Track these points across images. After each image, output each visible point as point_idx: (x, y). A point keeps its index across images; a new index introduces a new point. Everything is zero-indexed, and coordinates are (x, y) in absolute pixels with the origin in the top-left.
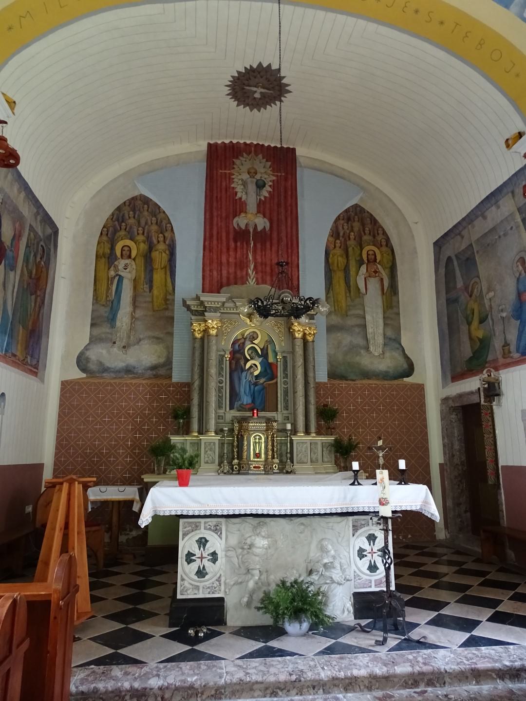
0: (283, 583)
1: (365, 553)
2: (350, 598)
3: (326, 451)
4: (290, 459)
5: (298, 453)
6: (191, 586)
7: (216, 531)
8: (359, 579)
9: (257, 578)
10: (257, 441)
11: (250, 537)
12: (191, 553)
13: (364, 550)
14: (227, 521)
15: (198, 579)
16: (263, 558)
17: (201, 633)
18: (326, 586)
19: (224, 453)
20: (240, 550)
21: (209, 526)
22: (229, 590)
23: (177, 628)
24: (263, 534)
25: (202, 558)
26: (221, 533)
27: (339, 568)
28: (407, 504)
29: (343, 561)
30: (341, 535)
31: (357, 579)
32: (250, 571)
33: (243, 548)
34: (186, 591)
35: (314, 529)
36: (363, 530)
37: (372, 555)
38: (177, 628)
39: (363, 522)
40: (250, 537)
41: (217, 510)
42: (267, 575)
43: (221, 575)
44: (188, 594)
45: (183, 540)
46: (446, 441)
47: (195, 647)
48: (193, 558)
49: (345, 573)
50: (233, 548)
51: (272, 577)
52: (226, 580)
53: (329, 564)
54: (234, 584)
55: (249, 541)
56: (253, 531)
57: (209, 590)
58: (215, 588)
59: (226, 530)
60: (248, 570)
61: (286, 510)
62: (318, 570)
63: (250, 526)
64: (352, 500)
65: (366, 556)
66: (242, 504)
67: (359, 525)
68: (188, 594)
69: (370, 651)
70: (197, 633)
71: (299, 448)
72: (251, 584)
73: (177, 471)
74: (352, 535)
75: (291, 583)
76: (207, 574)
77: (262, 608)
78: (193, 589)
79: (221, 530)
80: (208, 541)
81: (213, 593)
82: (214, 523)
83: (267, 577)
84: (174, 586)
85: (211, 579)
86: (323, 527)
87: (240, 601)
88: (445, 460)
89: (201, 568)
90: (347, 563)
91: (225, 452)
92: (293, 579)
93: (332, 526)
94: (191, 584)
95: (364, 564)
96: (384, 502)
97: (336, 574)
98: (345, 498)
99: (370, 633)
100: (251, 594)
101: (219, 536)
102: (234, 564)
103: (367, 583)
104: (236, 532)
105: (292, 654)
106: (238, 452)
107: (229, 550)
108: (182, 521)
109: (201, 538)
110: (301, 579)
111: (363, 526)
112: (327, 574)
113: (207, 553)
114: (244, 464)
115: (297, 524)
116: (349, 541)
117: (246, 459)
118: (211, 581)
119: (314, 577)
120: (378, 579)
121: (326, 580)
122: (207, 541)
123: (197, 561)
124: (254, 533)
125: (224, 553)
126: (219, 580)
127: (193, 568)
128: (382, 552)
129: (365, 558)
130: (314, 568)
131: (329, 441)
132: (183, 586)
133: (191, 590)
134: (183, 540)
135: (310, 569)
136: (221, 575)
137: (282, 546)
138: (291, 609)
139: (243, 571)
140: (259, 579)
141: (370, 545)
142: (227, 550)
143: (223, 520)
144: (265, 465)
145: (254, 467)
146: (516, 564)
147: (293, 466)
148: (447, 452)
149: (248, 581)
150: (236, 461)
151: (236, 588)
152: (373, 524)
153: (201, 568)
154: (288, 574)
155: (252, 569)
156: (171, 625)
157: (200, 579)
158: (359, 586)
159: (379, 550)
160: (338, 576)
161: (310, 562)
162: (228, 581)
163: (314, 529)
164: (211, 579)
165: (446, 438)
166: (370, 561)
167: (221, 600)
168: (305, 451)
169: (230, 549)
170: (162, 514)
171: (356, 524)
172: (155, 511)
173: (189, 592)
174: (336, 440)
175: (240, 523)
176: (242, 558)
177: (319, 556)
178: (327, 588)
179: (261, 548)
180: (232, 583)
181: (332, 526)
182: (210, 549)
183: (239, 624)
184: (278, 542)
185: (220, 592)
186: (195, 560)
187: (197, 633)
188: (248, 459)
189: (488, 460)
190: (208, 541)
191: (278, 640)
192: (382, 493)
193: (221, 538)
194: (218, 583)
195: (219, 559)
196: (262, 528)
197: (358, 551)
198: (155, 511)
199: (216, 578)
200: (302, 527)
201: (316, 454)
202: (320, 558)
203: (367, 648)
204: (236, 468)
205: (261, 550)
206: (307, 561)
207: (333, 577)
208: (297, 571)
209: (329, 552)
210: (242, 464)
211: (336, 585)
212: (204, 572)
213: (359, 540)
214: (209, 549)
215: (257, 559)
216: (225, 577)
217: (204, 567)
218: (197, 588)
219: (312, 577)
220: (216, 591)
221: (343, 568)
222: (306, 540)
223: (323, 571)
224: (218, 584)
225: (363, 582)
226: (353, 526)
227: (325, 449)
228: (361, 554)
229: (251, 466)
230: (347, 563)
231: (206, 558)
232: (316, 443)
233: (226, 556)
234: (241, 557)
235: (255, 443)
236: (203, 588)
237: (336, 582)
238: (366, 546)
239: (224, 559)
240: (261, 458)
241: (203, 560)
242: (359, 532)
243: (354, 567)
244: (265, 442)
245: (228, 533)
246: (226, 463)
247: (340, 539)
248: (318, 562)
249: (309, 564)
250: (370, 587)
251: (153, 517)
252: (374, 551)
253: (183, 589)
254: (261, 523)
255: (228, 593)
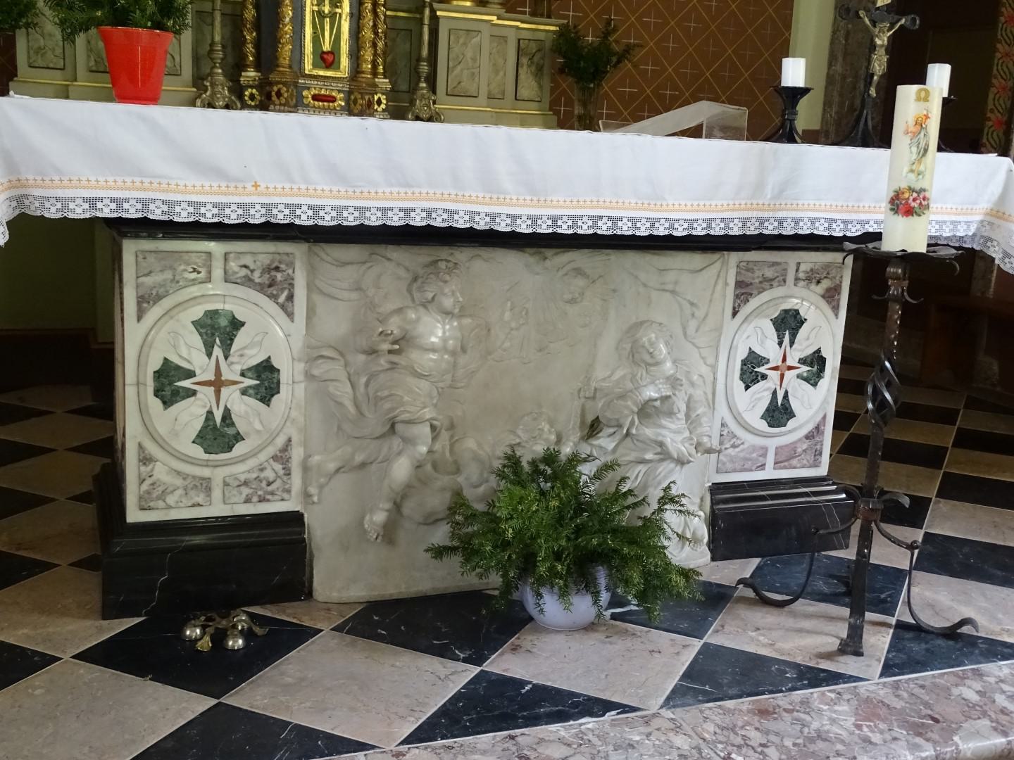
0: (513, 461)
1: (762, 370)
2: (702, 499)
3: (529, 66)
4: (427, 80)
5: (451, 64)
6: (179, 482)
7: (274, 291)
8: (734, 446)
9: (424, 449)
10: (327, 9)
11: (400, 311)
12: (178, 368)
13: (762, 361)
14: (309, 248)
15: (207, 456)
16: (441, 385)
17: (235, 637)
18: (642, 468)
19: (212, 44)
20: (362, 358)
21: (244, 272)
22: (321, 487)
23: (137, 620)
24: (448, 303)
25: (218, 384)
26: (290, 298)
27: (682, 415)
28: (946, 218)
29: (698, 394)
30: (697, 313)
31: (728, 446)
32: (399, 427)
33: (372, 352)
34: (162, 496)
35: (614, 291)
36: (766, 296)
37: (782, 376)
38: (137, 620)
39: (769, 273)
40: (400, 311)
41: (293, 208)
42: (452, 437)
43: (290, 440)
44: (169, 507)
45: (139, 319)
46: (838, 68)
47: (231, 699)
48: (186, 384)
49: (699, 430)
50: (330, 346)
51: (470, 444)
52: (307, 457)
53: (658, 404)
54: (338, 470)
55: (394, 326)
56: (409, 291)
57: (246, 491)
58: (269, 484)
59: (311, 287)
60: (393, 426)
61: (554, 219)
62: (621, 421)
63: (402, 273)
64: (780, 194)
65: (764, 377)
66: (395, 190)
67: (757, 281)
68: (169, 507)
69: (834, 678)
70: (219, 638)
71: (456, 49)
72: (401, 470)
73: (106, 38)
74: (729, 311)
75: (533, 463)
76: (238, 437)
77: (452, 550)
78: (185, 489)
79: (292, 285)
80: (243, 324)
81: (262, 500)
82: (265, 260)
83: (452, 446)
84: (95, 463)
85: (254, 454)
86: (645, 285)
87: (361, 524)
88: (824, 120)
89: (218, 419)
90: (707, 399)
91: (218, 38)
92: (539, 449)
93: (676, 283)
94: (178, 473)
95: (754, 402)
96: (913, 204)
97: (674, 434)
98: (759, 186)
99: (787, 608)
100: (398, 500)
101: (283, 307)
102: (340, 404)
103: (754, 455)
104: (346, 295)
105: (595, 707)
106: (258, 44)
107: (322, 357)
108: (130, 249)
109: (213, 314)
110: (567, 450)
111: (766, 285)
112: (649, 432)
113: (238, 368)
114: (285, 84)
115: (561, 273)
116: (719, 330)
117: (290, 67)
118: (252, 463)
119: (605, 442)
120: (787, 446)
121: (645, 451)
122: (236, 324)
123: (199, 395)
124: (413, 300)
125: (300, 366)
126: (282, 457)
127: (184, 418)
128: (811, 365)
129: (762, 384)
130: (608, 414)
131: (542, 36)
132: (149, 481)
133: (180, 492)
134: (139, 319)
135: (590, 418)
136: (290, 440)
137: (507, 344)
138: (568, 554)
139: (374, 424)
140: (430, 452)
141: (780, 344)
142: (313, 356)
143: (296, 250)
144: (350, 93)
145: (315, 98)
146: (998, 389)
147: (434, 103)
148: (836, 99)
149: (388, 460)
150: (251, 74)
151: (342, 482)
152: (797, 279)
153: (218, 419)
154: (520, 433)
155: (409, 422)
156: (110, 611)
157: (213, 457)
158: (729, 466)
159: (803, 361)
160: (679, 438)
161: (594, 398)
162: (316, 459)
163: (614, 291)
164: (254, 454)
165: (840, 59)
166: (775, 393)
167: (295, 519)
168: (474, 60)
169: (325, 353)
170: (53, 213)
171: (747, 277)
172: (20, 200)
173: (171, 500)
174: (563, 33)
175: (364, 263)
176: (367, 385)
177: (623, 377)
178: (641, 475)
179: (434, 350)
180: (332, 466)
181: (676, 283)
182: (249, 352)
183: (360, 591)
184: (492, 331)
185: (286, 496)
186: (194, 393)
187: (219, 638)
188: (296, 68)
189: (989, 119)
190: (243, 324)
191: (515, 649)
192: (912, 171)
193: (290, 315)
194: (278, 467)
195: (283, 388)
196: (446, 282)
197: (744, 363)
198: (20, 200)
199: (271, 451)
200: (580, 282)
201: (501, 73)
202: (629, 386)
203: (812, 664)
204: (252, 97)
205: (433, 356)
206: (582, 394)
207: (668, 441)
208: (551, 423)
209: (657, 364)
210: (279, 83)
211: (672, 465)
212: (231, 431)
213: (749, 329)
214: (248, 351)
215: (424, 385)
216: (305, 447)
217: (227, 416)
218: (205, 485)
219: (595, 442)
220: (272, 493)
221: (693, 416)
222: (585, 326)
223: (632, 423)
224: (281, 472)
225: (742, 455)
226: (739, 284)
227: (524, 61)
228: (752, 371)
229: (305, 93)
230: (707, 399)
231: (235, 383)
232: (504, 38)
233: (309, 376)
234: (363, 380)
235: (321, 15)
236: (226, 484)
237: (676, 456)
238: (770, 349)
239: (303, 385)
240: (338, 68)
241: (223, 390)
242: (754, 303)
243: (722, 411)
244: (351, 15)
245: (317, 298)
246: (221, 78)
247: (692, 325)
248: (622, 397)
249: (589, 404)
250: (762, 467)
251: (10, 224)
252: (789, 362)
253: (148, 492)
254: (442, 265)
255: (315, 499)
